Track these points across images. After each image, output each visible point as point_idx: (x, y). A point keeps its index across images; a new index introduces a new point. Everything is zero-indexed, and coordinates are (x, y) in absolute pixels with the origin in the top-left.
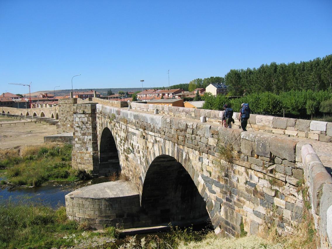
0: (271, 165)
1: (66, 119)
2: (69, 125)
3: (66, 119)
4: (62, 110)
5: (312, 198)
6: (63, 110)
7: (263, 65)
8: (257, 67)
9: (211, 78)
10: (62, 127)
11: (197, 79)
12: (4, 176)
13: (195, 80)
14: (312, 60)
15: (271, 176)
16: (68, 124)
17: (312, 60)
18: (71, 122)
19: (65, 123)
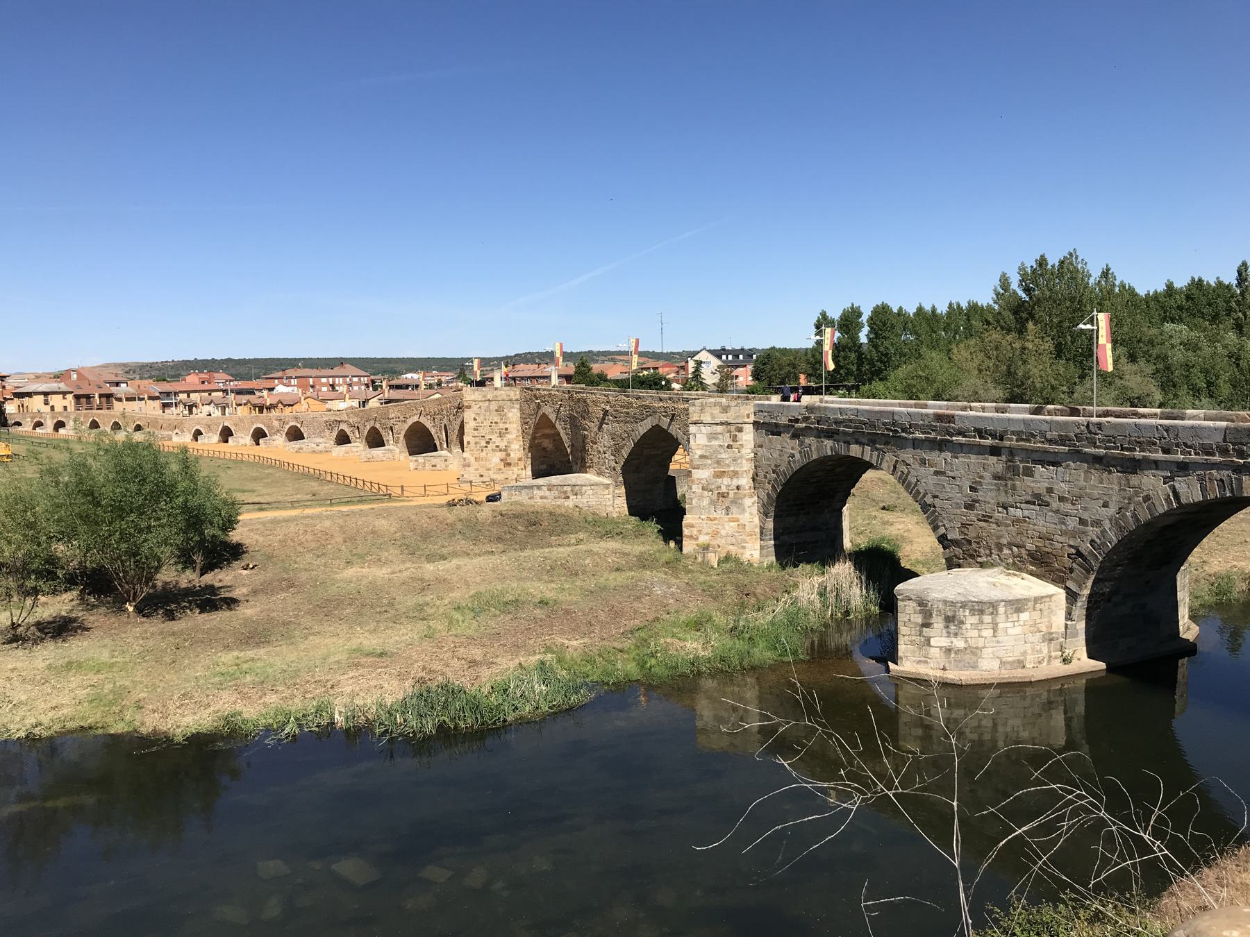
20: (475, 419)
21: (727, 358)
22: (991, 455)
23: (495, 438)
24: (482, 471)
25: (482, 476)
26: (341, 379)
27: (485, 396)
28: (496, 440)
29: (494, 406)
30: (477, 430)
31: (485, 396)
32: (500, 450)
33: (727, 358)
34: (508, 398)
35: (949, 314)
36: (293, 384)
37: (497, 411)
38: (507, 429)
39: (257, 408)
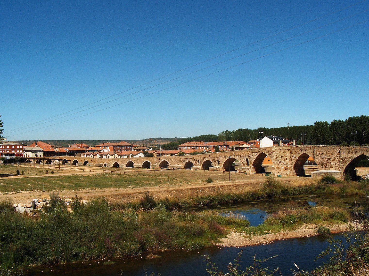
0: (10, 141)
1: (280, 163)
2: (283, 168)
3: (280, 163)
4: (276, 155)
5: (23, 166)
6: (277, 156)
7: (335, 121)
8: (311, 123)
9: (240, 130)
10: (276, 169)
11: (225, 131)
12: (1, 147)
13: (223, 132)
14: (355, 117)
15: (81, 166)
16: (282, 166)
17: (355, 117)
18: (286, 165)
19: (279, 166)
20: (276, 155)
21: (274, 140)
22: (353, 181)
23: (283, 161)
24: (278, 171)
25: (278, 173)
26: (108, 147)
27: (279, 148)
28: (283, 161)
29: (282, 151)
30: (277, 159)
31: (279, 148)
32: (284, 165)
33: (274, 140)
34: (287, 149)
35: (315, 125)
36: (107, 148)
37: (283, 153)
38: (286, 158)
39: (119, 156)
